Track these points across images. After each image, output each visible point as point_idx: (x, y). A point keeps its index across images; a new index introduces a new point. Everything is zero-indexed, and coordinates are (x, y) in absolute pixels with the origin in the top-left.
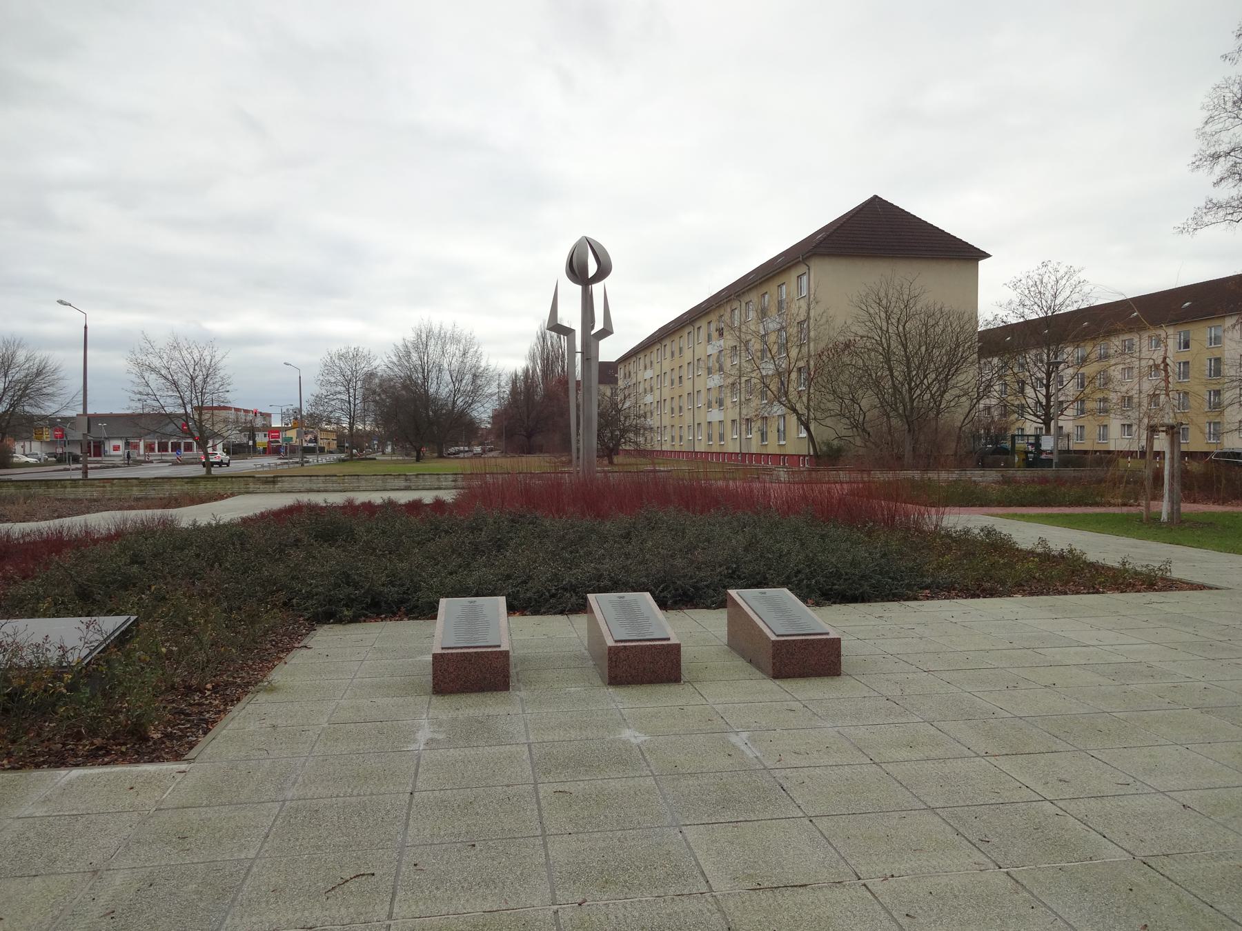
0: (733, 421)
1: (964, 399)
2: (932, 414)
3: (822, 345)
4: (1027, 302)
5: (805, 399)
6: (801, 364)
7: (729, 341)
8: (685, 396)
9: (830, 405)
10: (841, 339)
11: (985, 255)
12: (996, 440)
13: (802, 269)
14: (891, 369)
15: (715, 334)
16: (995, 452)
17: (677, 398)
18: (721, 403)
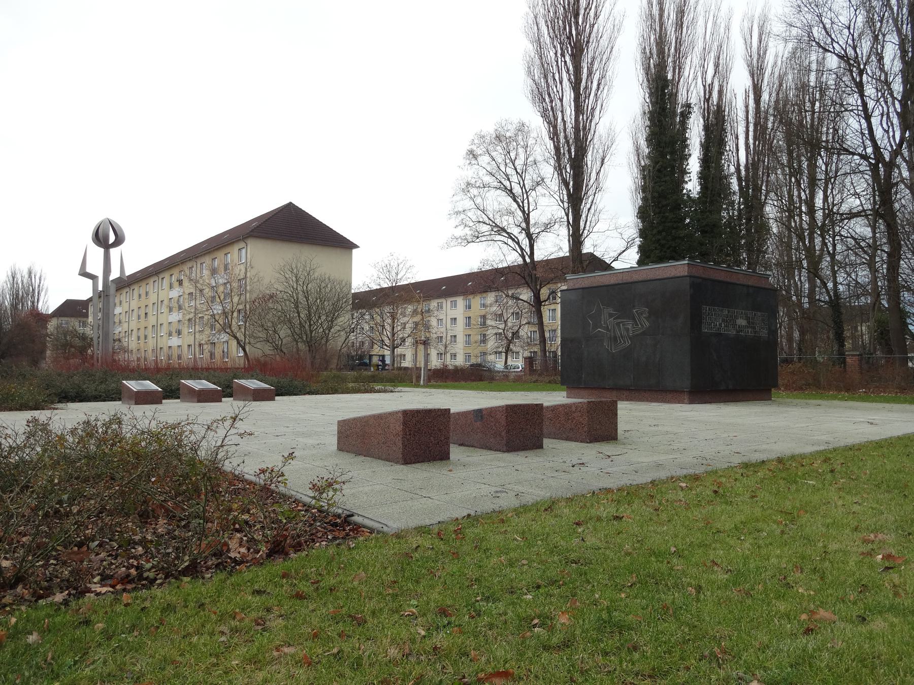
0: (189, 346)
1: (342, 333)
2: (323, 342)
3: (254, 296)
4: (382, 276)
5: (243, 330)
6: (241, 307)
7: (188, 287)
8: (150, 328)
9: (260, 335)
10: (268, 292)
11: (356, 246)
12: (361, 358)
13: (242, 245)
14: (298, 313)
15: (176, 284)
16: (360, 365)
17: (142, 329)
18: (179, 333)
